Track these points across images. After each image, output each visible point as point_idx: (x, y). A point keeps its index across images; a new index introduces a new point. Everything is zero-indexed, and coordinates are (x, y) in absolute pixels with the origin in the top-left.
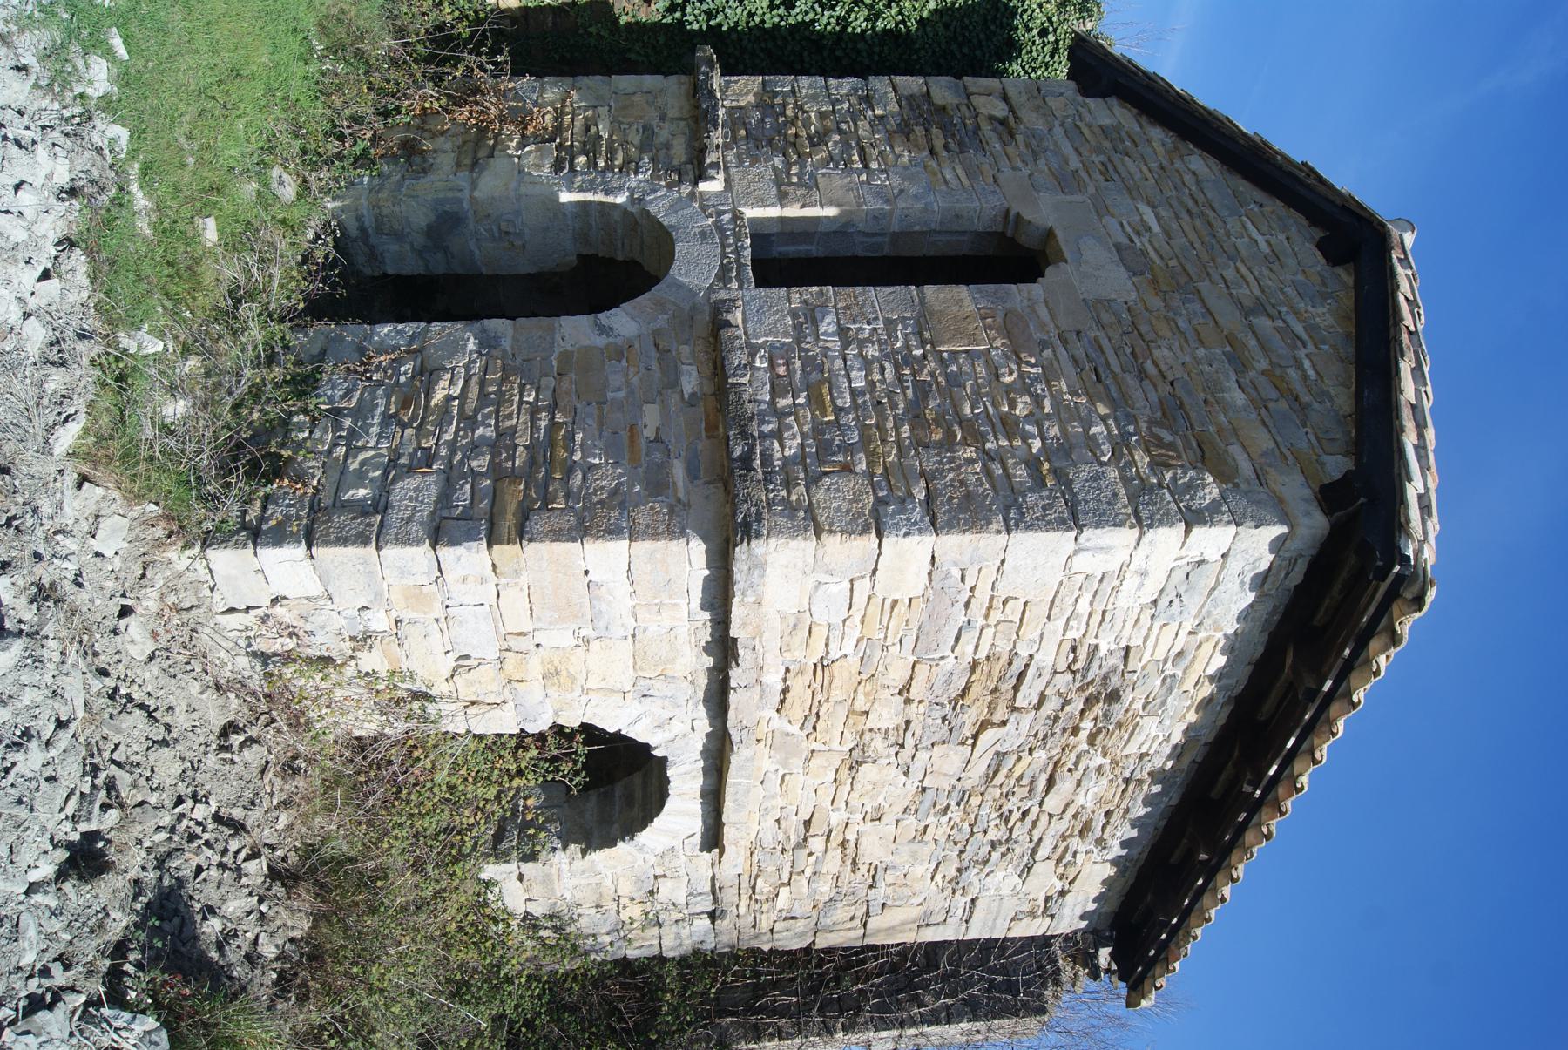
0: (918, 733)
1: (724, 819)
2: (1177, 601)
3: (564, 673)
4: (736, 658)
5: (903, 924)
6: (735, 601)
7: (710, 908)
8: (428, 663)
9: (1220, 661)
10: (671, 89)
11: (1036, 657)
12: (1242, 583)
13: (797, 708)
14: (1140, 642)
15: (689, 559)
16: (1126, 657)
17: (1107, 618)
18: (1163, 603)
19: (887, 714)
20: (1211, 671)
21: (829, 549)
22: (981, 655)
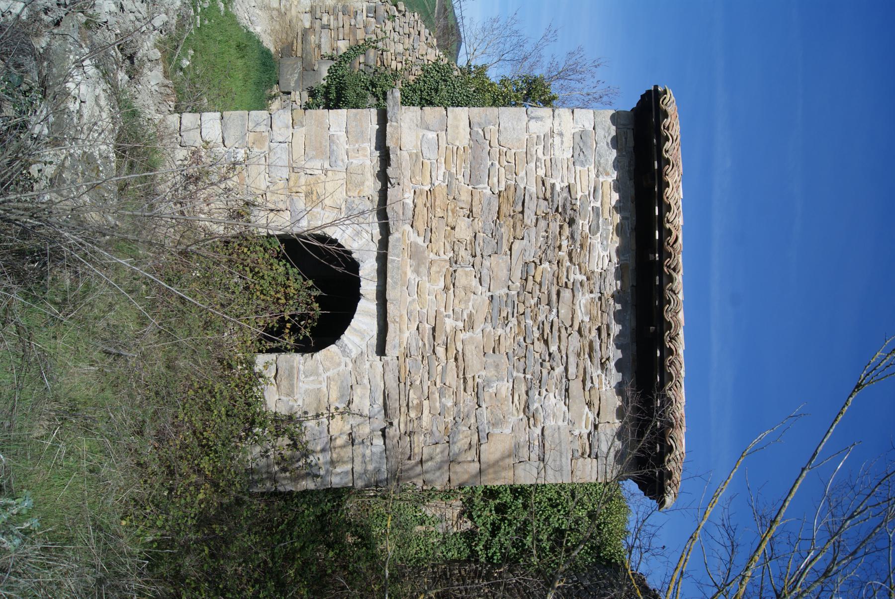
0: (482, 244)
1: (388, 298)
2: (581, 154)
3: (315, 193)
4: (390, 165)
5: (503, 458)
6: (388, 124)
7: (377, 103)
8: (257, 180)
9: (616, 196)
10: (525, 109)
11: (527, 187)
12: (607, 144)
13: (421, 225)
14: (573, 182)
15: (372, 114)
16: (569, 191)
17: (553, 162)
18: (576, 155)
19: (464, 231)
20: (613, 203)
21: (426, 112)
22: (502, 188)
